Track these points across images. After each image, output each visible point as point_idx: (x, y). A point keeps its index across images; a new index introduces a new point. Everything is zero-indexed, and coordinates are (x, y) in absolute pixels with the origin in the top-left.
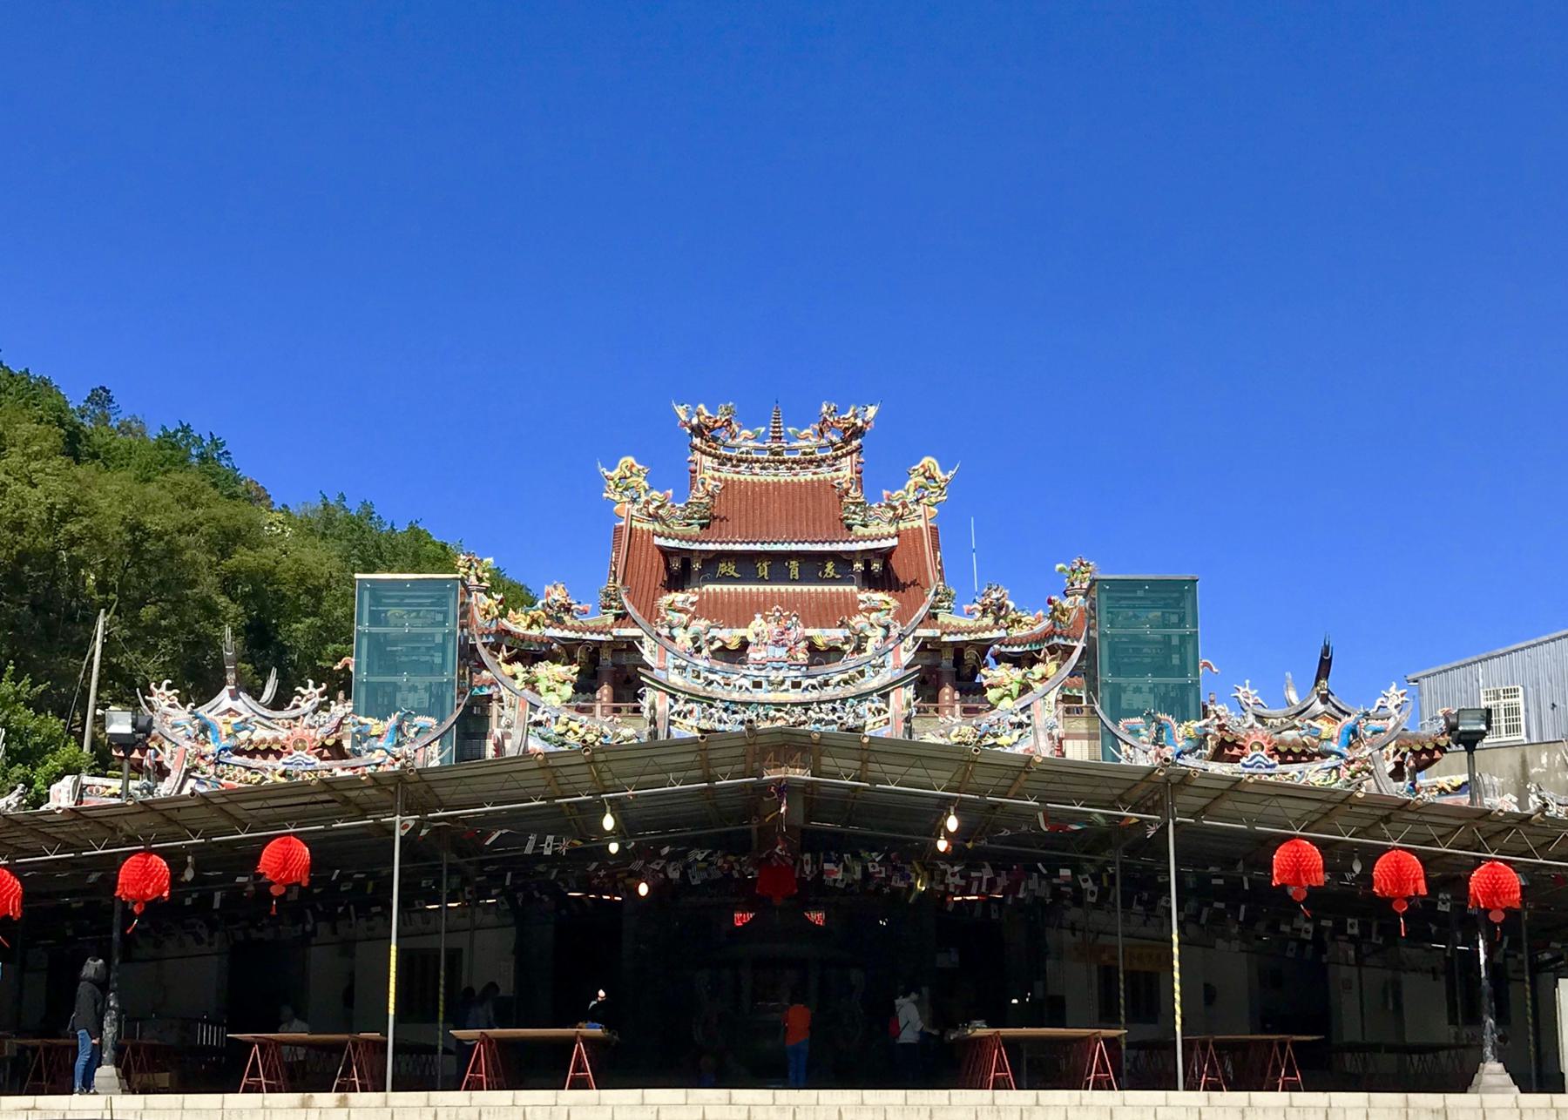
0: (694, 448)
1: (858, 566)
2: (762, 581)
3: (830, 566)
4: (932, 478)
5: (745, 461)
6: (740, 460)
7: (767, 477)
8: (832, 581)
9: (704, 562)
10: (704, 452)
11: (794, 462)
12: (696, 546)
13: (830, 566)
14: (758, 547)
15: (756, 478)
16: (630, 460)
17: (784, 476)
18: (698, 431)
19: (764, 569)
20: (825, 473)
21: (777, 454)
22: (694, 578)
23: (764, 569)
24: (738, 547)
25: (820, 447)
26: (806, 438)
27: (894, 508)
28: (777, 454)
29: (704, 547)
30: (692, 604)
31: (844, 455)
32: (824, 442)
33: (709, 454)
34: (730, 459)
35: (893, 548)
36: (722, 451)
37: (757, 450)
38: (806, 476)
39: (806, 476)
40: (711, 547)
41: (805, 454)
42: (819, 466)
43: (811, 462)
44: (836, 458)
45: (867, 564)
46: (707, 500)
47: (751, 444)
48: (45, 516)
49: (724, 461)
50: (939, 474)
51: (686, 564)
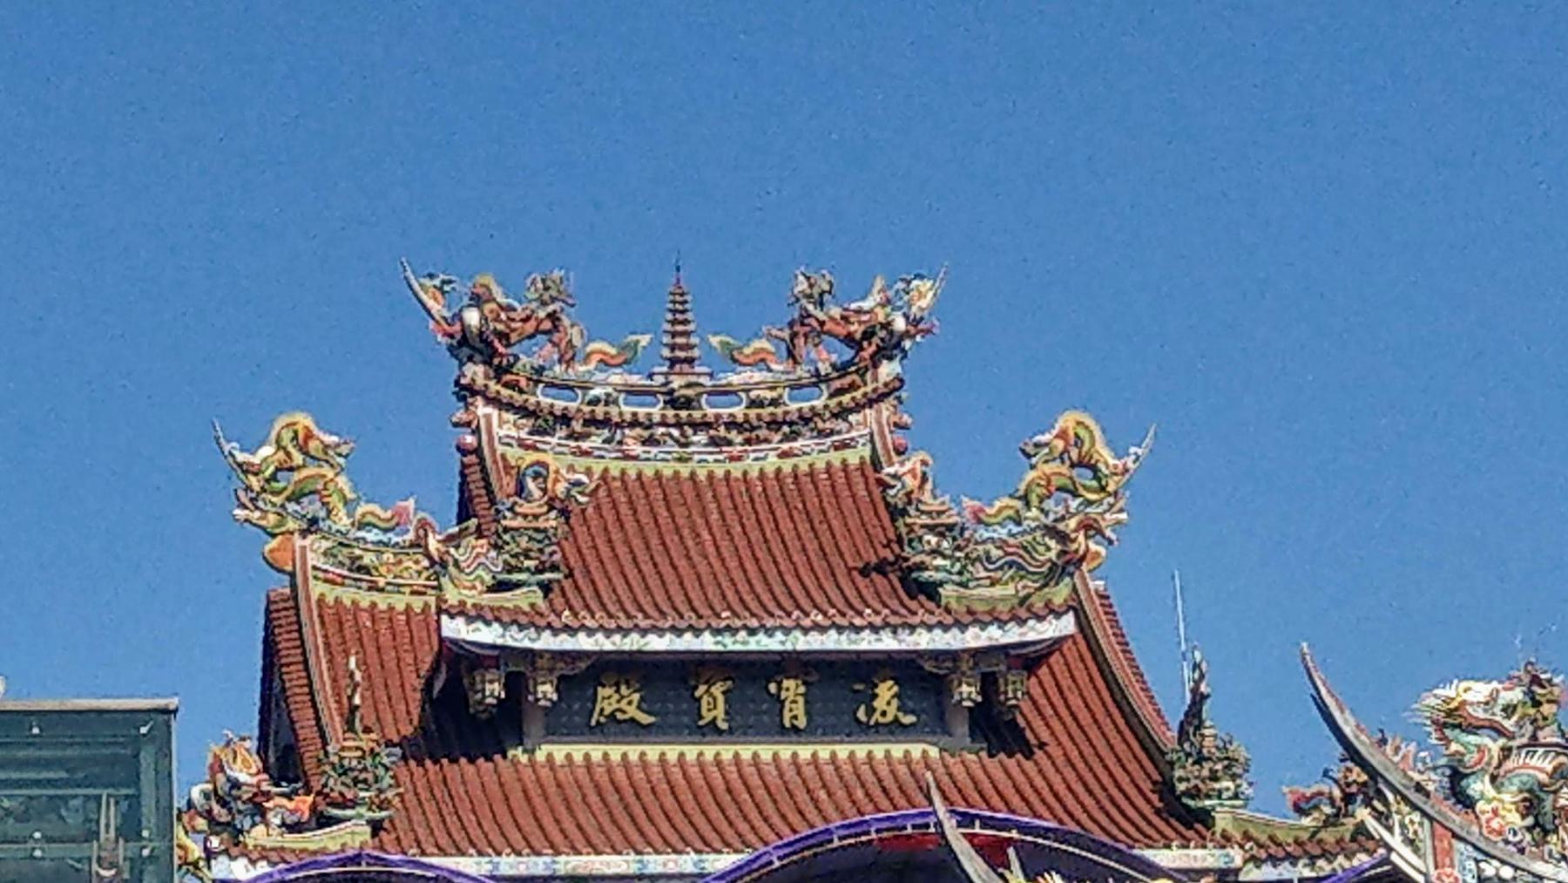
0: (466, 392)
1: (968, 692)
2: (711, 732)
3: (886, 691)
4: (1086, 464)
5: (606, 422)
6: (591, 422)
7: (660, 463)
8: (895, 730)
9: (563, 684)
10: (494, 401)
11: (732, 424)
12: (547, 642)
13: (886, 691)
14: (707, 643)
15: (632, 468)
16: (304, 420)
17: (706, 463)
18: (469, 345)
19: (714, 701)
20: (812, 454)
21: (688, 403)
22: (534, 727)
23: (714, 701)
24: (656, 643)
25: (796, 386)
26: (761, 362)
27: (1063, 538)
28: (688, 403)
29: (565, 643)
30: (1509, 710)
31: (858, 407)
32: (802, 372)
33: (509, 406)
34: (565, 419)
35: (1057, 644)
36: (542, 398)
37: (632, 391)
38: (766, 460)
39: (766, 460)
40: (584, 642)
41: (756, 403)
42: (794, 436)
43: (774, 425)
44: (842, 413)
45: (989, 684)
46: (551, 521)
47: (617, 378)
48: (510, 416)
49: (544, 422)
50: (1105, 457)
51: (516, 685)
